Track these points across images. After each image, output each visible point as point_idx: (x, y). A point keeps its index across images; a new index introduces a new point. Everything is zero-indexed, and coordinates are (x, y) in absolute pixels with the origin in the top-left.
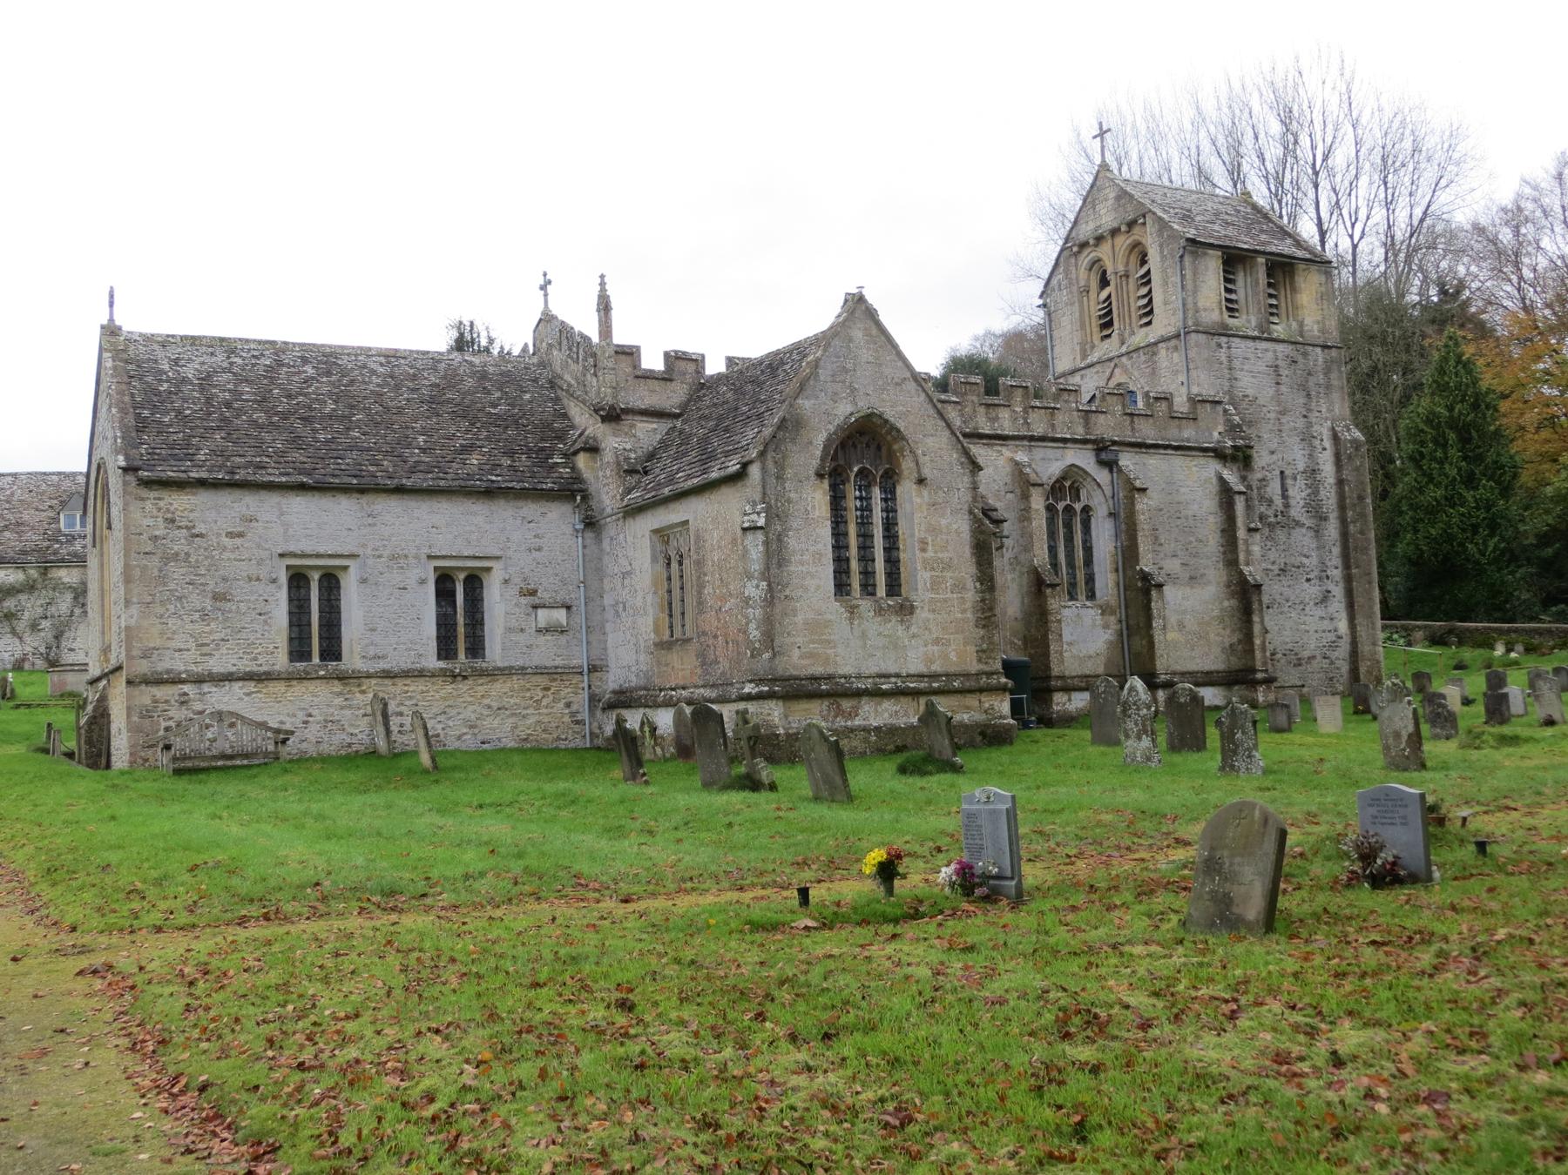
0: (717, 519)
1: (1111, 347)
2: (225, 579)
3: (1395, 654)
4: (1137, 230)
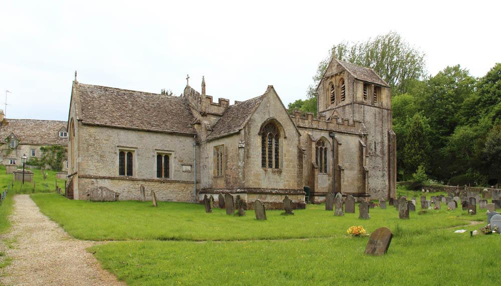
0: (232, 144)
1: (334, 106)
2: (103, 151)
3: (399, 191)
4: (342, 74)
